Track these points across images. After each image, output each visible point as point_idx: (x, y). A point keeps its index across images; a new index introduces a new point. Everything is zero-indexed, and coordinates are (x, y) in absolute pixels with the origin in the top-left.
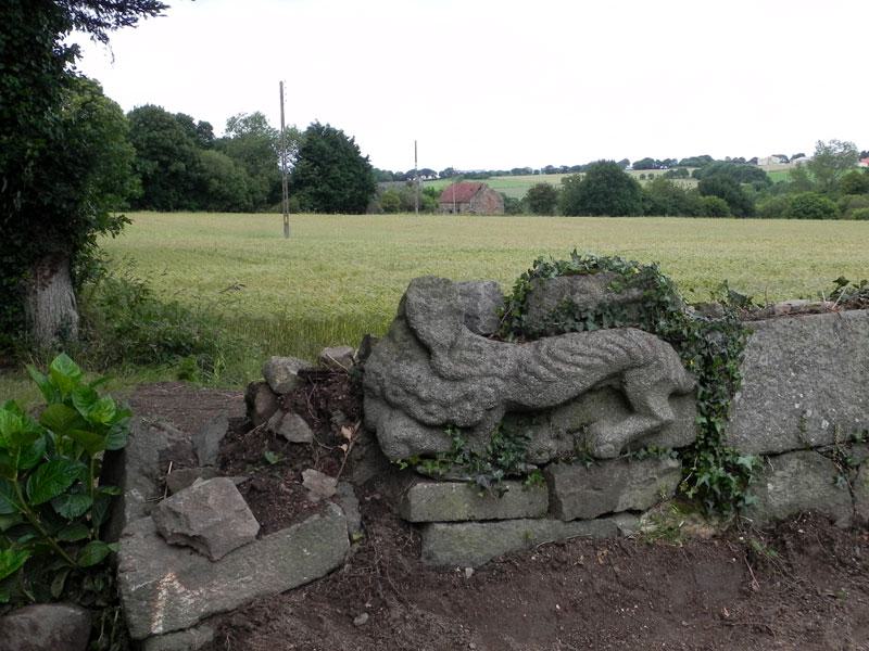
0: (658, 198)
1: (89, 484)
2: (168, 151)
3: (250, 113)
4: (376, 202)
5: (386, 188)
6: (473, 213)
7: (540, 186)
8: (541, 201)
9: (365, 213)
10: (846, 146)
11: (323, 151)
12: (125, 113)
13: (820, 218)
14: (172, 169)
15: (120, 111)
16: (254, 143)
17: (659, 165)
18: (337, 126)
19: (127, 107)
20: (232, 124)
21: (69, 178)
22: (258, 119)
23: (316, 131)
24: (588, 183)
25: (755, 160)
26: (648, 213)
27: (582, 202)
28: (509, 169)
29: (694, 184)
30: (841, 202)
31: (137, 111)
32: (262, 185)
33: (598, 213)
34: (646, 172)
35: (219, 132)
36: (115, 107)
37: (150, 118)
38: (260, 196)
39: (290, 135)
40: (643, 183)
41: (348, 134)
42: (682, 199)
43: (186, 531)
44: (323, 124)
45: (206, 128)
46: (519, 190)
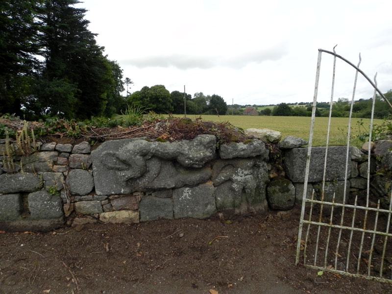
0: (296, 112)
1: (40, 11)
2: (180, 101)
3: (199, 92)
4: (227, 112)
5: (229, 109)
6: (251, 115)
7: (267, 109)
8: (266, 112)
9: (224, 115)
10: (346, 99)
11: (215, 101)
12: (170, 92)
13: (337, 117)
14: (181, 105)
15: (119, 86)
16: (200, 99)
17: (305, 104)
18: (219, 95)
19: (150, 87)
20: (195, 95)
21: (387, 196)
22: (201, 94)
23: (214, 96)
24: (279, 108)
25: (328, 103)
26: (294, 115)
27: (277, 113)
28: (269, 105)
29: (306, 108)
30: (343, 113)
31: (173, 92)
32: (201, 108)
33: (281, 115)
34: (301, 106)
35: (193, 97)
36: (168, 92)
37: (176, 93)
38: (200, 111)
39: (209, 97)
40: (293, 108)
41: (222, 97)
42: (302, 112)
43: (161, 143)
44: (216, 95)
45: (190, 96)
46: (260, 110)
